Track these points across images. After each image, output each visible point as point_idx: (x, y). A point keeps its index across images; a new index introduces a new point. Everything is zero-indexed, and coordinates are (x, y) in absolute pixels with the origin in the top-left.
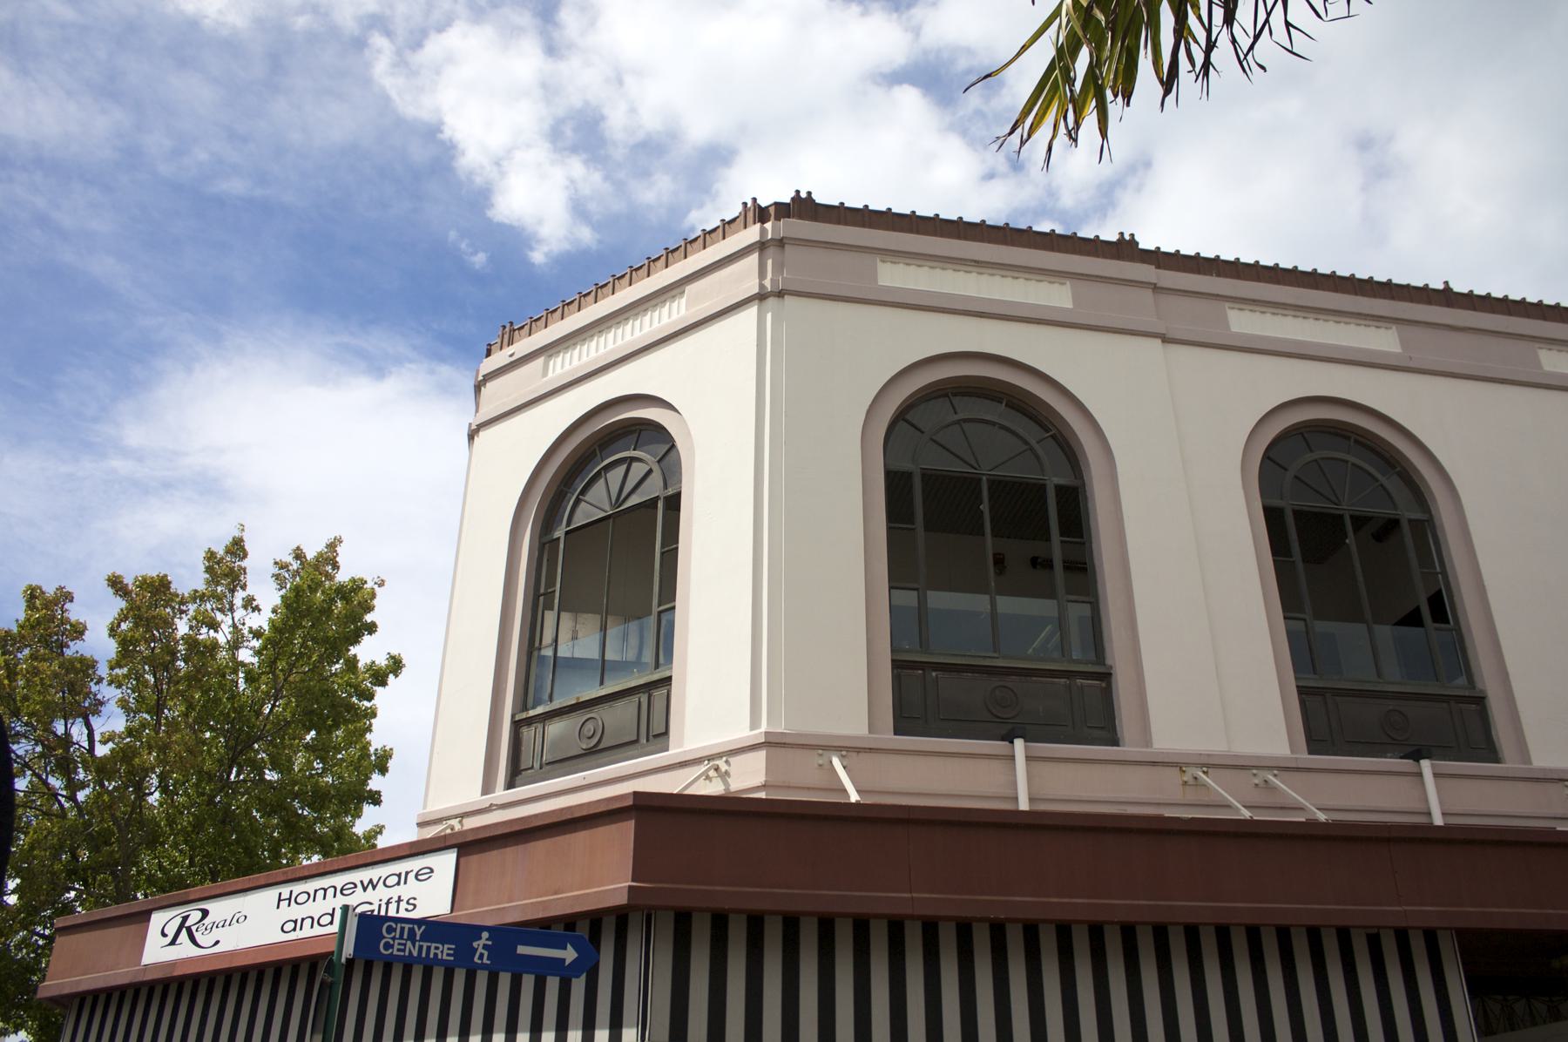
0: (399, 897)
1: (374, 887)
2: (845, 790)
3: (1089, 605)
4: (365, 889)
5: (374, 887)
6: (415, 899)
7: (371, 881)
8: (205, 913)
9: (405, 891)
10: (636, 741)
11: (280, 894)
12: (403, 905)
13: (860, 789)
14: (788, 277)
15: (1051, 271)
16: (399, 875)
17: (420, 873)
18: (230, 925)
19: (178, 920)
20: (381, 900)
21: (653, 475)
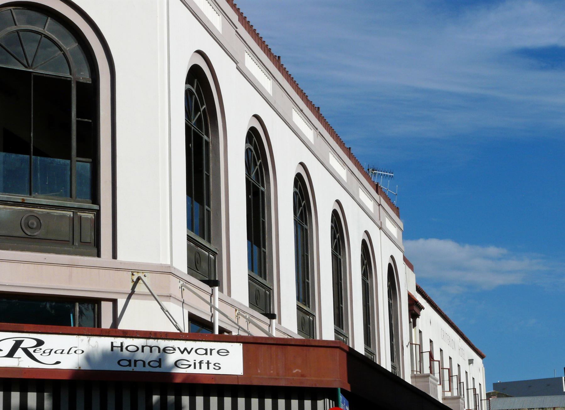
0: (208, 361)
1: (189, 353)
2: (219, 320)
3: (444, 367)
4: (182, 353)
5: (189, 353)
6: (219, 364)
7: (185, 349)
8: (40, 343)
9: (214, 358)
10: (81, 242)
11: (112, 343)
12: (211, 366)
13: (220, 319)
14: (261, 159)
15: (376, 224)
16: (206, 350)
17: (220, 351)
18: (68, 353)
19: (11, 343)
20: (41, 355)
21: (69, 74)
